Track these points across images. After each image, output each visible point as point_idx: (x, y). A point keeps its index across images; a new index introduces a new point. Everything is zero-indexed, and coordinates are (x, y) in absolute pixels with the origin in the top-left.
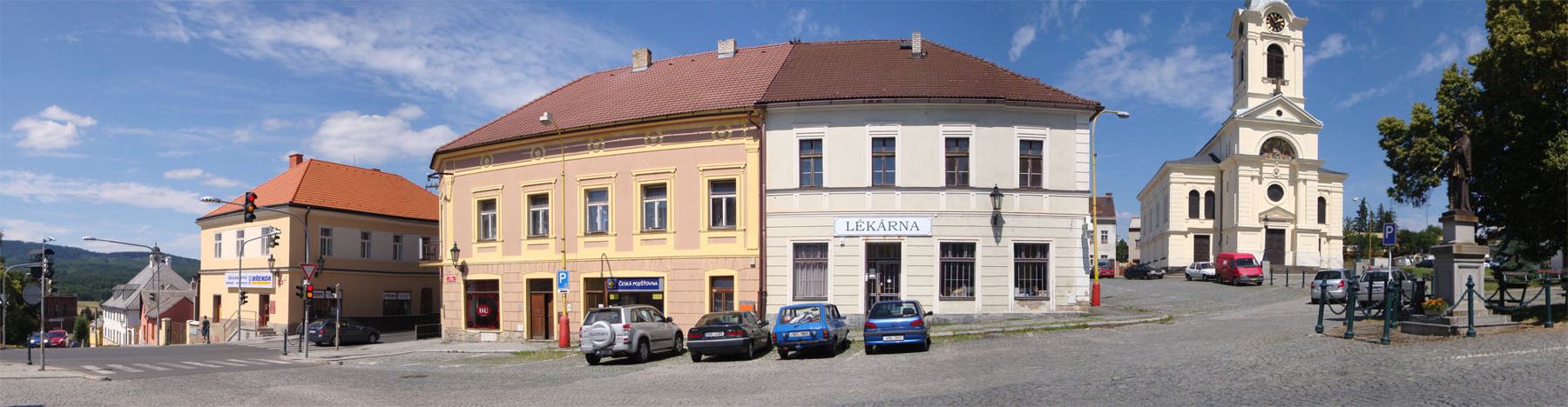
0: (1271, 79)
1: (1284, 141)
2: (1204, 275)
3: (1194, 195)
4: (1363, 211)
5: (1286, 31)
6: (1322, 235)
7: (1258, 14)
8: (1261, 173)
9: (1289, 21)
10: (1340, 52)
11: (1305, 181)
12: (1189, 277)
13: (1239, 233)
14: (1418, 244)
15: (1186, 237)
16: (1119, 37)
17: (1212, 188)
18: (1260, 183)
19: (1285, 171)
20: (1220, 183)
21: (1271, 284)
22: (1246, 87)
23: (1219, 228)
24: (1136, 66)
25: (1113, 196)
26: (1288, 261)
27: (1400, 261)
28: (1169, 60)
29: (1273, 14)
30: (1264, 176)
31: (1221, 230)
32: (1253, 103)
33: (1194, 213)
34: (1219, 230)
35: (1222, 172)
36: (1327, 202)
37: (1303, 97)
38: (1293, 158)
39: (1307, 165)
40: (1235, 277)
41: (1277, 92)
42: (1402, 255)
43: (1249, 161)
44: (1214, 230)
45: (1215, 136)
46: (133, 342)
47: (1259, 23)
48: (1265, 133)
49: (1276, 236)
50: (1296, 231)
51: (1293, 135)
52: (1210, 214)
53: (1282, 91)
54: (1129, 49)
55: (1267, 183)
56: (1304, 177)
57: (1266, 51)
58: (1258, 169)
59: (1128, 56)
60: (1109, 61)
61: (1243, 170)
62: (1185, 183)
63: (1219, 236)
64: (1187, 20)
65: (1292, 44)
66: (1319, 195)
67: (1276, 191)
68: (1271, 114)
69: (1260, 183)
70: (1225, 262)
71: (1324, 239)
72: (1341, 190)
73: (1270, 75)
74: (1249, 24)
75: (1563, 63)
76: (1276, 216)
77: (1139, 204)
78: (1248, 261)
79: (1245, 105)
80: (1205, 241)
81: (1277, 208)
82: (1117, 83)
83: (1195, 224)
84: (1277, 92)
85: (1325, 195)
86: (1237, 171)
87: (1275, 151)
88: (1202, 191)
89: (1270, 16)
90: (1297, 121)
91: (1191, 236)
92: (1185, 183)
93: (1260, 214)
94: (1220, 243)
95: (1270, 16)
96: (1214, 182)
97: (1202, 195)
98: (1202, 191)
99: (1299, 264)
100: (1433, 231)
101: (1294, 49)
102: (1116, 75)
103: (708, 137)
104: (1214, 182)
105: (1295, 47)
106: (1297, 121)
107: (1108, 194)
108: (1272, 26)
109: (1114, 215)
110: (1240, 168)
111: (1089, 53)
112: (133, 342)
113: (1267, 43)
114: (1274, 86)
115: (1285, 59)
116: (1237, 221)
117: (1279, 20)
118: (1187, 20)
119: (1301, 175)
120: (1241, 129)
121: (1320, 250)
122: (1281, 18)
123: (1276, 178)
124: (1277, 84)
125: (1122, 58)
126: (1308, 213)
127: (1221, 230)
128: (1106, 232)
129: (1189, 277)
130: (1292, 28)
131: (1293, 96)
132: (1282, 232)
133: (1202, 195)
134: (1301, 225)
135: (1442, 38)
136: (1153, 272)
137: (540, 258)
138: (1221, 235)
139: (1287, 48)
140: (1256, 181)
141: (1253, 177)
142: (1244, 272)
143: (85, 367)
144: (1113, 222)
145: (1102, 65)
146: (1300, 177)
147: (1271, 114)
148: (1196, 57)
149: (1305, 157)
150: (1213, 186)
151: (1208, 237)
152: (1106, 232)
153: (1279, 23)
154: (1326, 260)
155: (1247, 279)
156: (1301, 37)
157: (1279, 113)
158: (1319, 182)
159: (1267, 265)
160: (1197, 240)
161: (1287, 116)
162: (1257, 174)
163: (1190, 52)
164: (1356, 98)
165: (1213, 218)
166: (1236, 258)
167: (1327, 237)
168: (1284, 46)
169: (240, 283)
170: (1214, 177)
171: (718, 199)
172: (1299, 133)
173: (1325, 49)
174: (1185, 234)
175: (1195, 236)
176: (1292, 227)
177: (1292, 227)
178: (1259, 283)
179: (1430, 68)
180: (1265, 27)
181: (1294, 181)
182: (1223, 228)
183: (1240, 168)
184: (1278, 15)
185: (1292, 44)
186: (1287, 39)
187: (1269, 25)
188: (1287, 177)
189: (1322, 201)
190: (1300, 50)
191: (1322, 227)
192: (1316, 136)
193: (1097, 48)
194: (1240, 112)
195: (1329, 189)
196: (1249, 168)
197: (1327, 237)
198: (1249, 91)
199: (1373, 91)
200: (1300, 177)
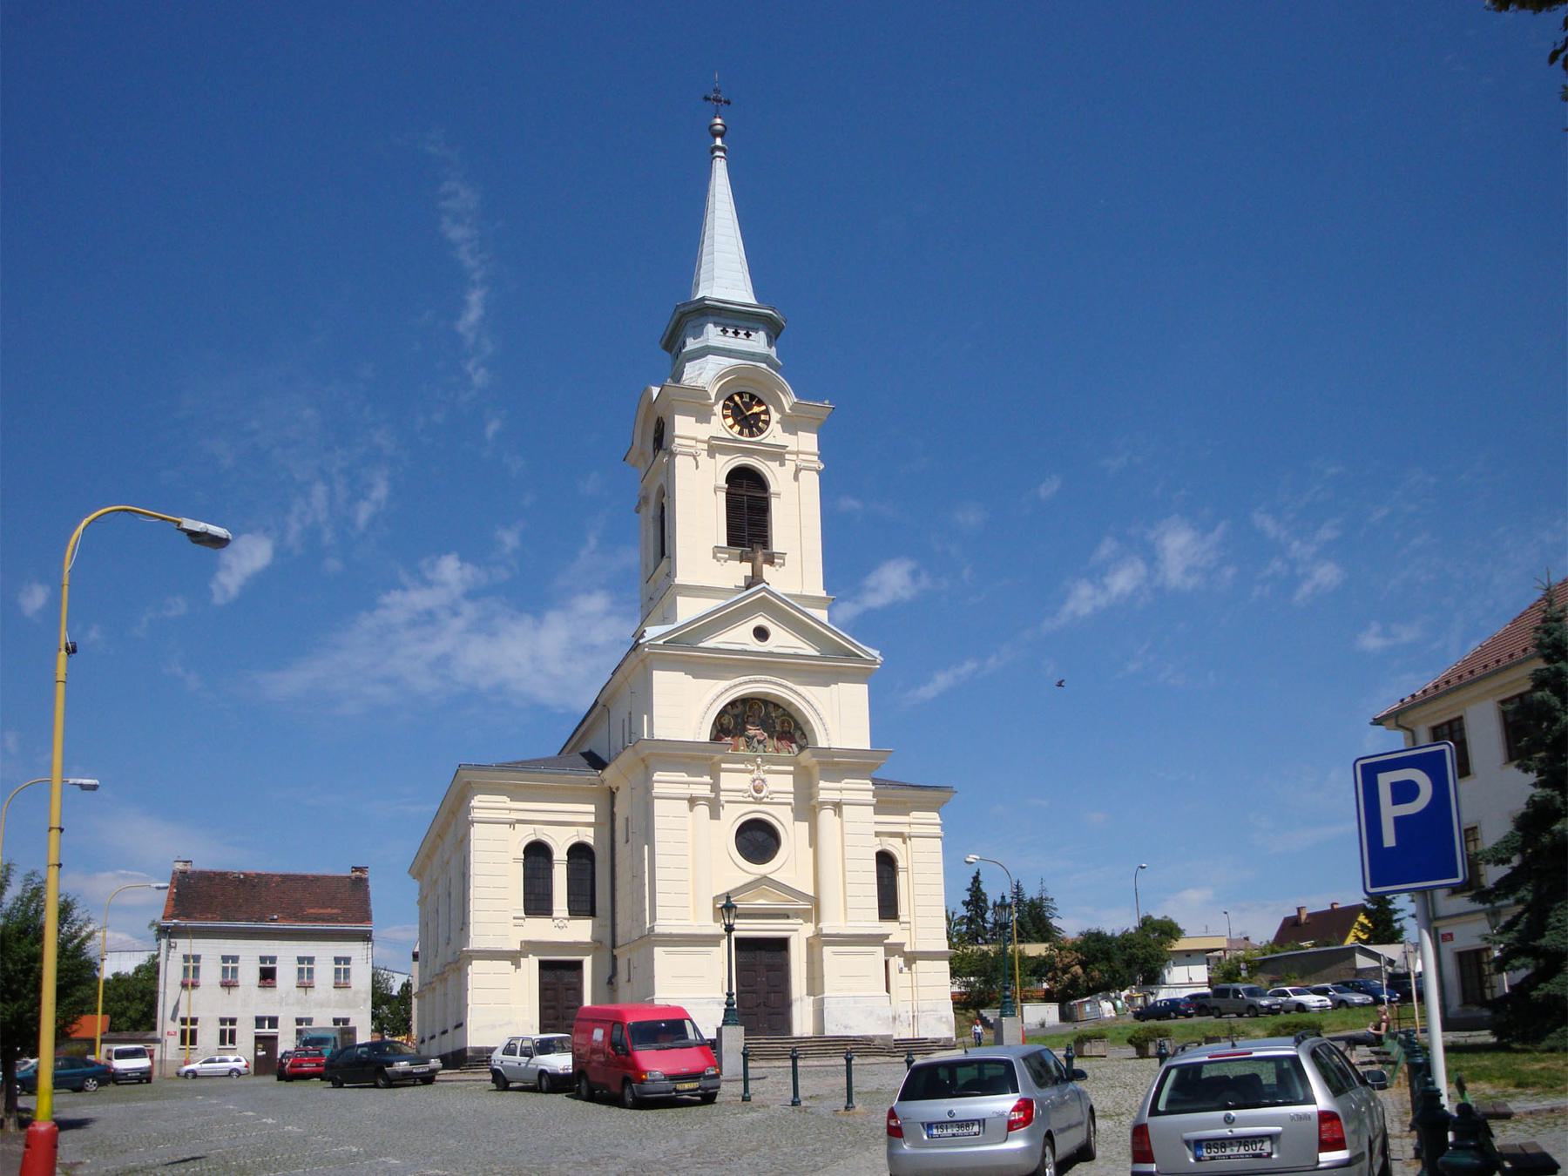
0: (737, 551)
1: (777, 706)
2: (542, 1073)
3: (537, 854)
4: (976, 899)
5: (774, 434)
6: (893, 950)
7: (702, 393)
8: (715, 788)
9: (780, 408)
10: (906, 595)
11: (837, 806)
12: (501, 1082)
13: (659, 952)
14: (1129, 963)
15: (518, 966)
16: (450, 569)
17: (588, 836)
18: (715, 814)
19: (781, 783)
20: (608, 821)
21: (746, 1099)
22: (671, 574)
23: (608, 942)
24: (484, 627)
25: (370, 875)
26: (802, 1023)
27: (1088, 1008)
28: (553, 617)
29: (740, 395)
30: (723, 797)
31: (614, 946)
32: (688, 610)
33: (537, 902)
34: (608, 946)
35: (612, 794)
36: (901, 863)
37: (823, 594)
38: (801, 748)
39: (842, 764)
40: (626, 1081)
41: (755, 580)
42: (1091, 992)
43: (681, 756)
44: (594, 947)
45: (596, 702)
47: (703, 416)
48: (723, 684)
49: (765, 957)
50: (819, 941)
51: (800, 689)
52: (582, 905)
53: (765, 577)
54: (472, 595)
55: (734, 817)
57: (723, 483)
58: (707, 779)
59: (469, 610)
60: (428, 618)
61: (666, 782)
62: (512, 824)
63: (608, 957)
64: (593, 542)
65: (790, 467)
66: (878, 845)
67: (760, 836)
68: (739, 637)
69: (715, 814)
70: (598, 1034)
71: (897, 962)
72: (937, 830)
73: (735, 538)
74: (678, 418)
75: (886, 941)
76: (761, 903)
77: (415, 885)
78: (672, 1028)
79: (669, 616)
80: (568, 976)
81: (765, 880)
82: (443, 661)
83: (541, 929)
84: (755, 580)
85: (893, 846)
86: (648, 785)
87: (752, 731)
88: (560, 845)
89: (731, 398)
90: (809, 650)
91: (531, 964)
92: (512, 824)
93: (715, 899)
94: (611, 981)
95: (731, 398)
96: (592, 819)
97: (560, 855)
98: (560, 845)
99: (832, 1030)
100: (1154, 930)
101: (796, 478)
102: (440, 646)
103: (822, 960)
104: (592, 819)
105: (798, 470)
106: (809, 650)
107: (357, 869)
108: (736, 422)
109: (366, 917)
110: (657, 776)
111: (387, 600)
113: (725, 464)
114: (746, 569)
115: (774, 503)
116: (653, 918)
117: (756, 409)
118: (593, 542)
119: (827, 791)
120: (658, 676)
121: (888, 990)
122: (760, 403)
123: (758, 801)
124: (752, 560)
125: (456, 613)
126: (851, 890)
127: (614, 946)
128: (347, 960)
129: (501, 1082)
130: (790, 426)
131: (796, 591)
132: (782, 945)
133: (560, 855)
134: (830, 925)
135: (1107, 548)
136: (402, 1066)
137: (265, 1002)
138: (614, 958)
139: (777, 477)
140: (703, 810)
141: (693, 801)
142: (656, 1064)
144: (366, 937)
145: (412, 624)
146: (823, 796)
147: (739, 637)
148: (609, 613)
149: (836, 744)
150: (591, 831)
151: (578, 966)
152: (347, 960)
153: (758, 414)
154: (906, 1016)
155: (668, 1085)
156: (815, 449)
158: (879, 810)
159: (735, 1039)
160: (550, 975)
161: (782, 640)
162: (705, 791)
163: (596, 603)
164: (942, 680)
165: (592, 913)
166: (630, 1021)
167: (904, 954)
168: (769, 469)
170: (592, 808)
172: (772, 461)
173: (875, 590)
174: (514, 957)
175: (541, 962)
176: (808, 929)
177: (808, 929)
178: (708, 1098)
179: (1086, 609)
180: (720, 425)
181: (807, 808)
182: (619, 941)
183: (657, 776)
184: (752, 397)
185: (790, 467)
186: (777, 454)
187: (730, 421)
188: (790, 798)
189: (886, 862)
190: (811, 482)
191: (888, 927)
192: (862, 689)
193: (404, 589)
194: (652, 632)
195: (905, 829)
196: (683, 777)
197: (904, 954)
198: (679, 580)
199: (970, 666)
200: (823, 796)
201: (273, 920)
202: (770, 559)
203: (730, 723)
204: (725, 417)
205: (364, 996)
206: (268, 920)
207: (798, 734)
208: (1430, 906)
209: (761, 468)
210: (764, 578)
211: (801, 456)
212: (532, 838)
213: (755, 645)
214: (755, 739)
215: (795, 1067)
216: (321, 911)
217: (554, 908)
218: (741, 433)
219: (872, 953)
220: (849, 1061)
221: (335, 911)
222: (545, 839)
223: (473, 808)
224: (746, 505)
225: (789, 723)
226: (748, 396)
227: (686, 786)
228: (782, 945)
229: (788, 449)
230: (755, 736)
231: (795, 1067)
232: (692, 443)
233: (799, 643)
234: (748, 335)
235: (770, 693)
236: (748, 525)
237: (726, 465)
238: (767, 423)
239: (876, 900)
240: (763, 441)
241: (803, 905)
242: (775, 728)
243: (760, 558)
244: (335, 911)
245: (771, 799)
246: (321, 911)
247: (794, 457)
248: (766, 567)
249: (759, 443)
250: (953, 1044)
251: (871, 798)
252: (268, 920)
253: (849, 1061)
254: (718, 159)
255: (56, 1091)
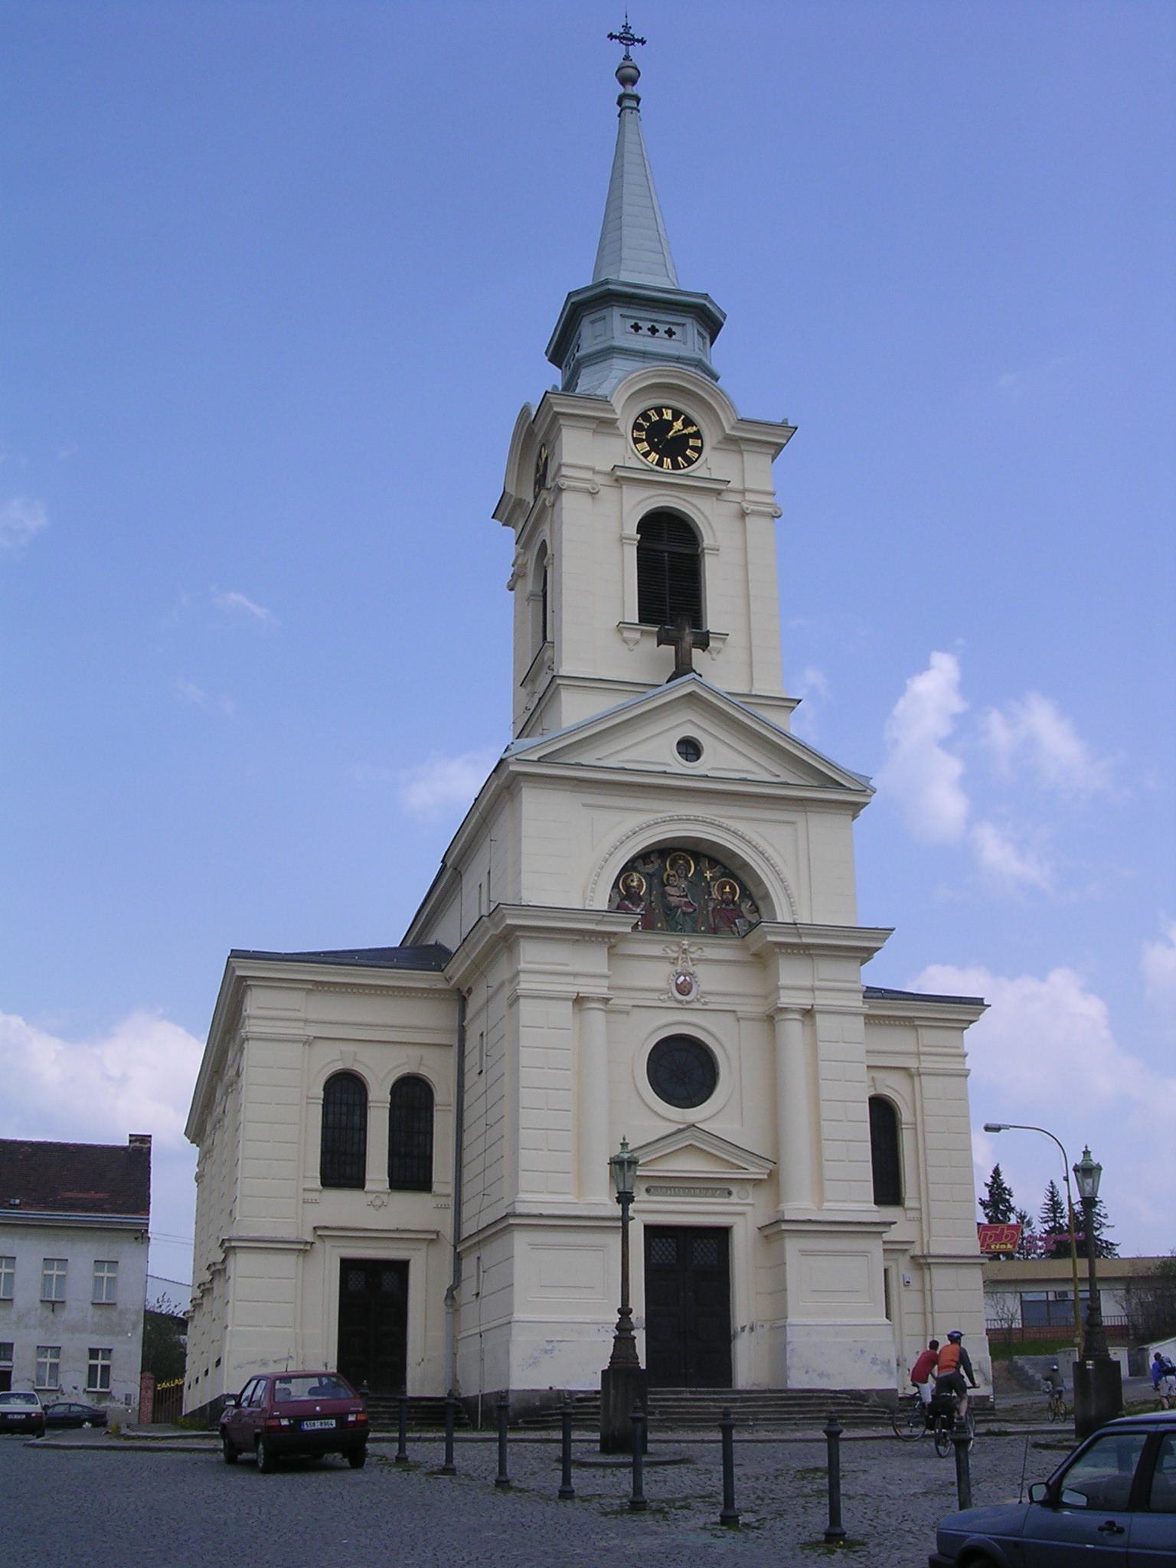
11: (808, 1013)
41: (683, 667)
46: (599, 1417)
50: (774, 1231)
56: (804, 1000)
57: (632, 530)
71: (902, 1268)
73: (647, 614)
85: (894, 1088)
92: (309, 1042)
108: (654, 448)
112: (599, 1417)
113: (639, 503)
123: (683, 1008)
134: (799, 1205)
143: (1111, 1422)
157: (690, 748)
168: (706, 515)
169: (566, 1442)
171: (94, 1359)
174: (303, 1249)
191: (889, 1213)
201: (15, 1206)
202: (703, 641)
203: (640, 885)
204: (636, 441)
205: (133, 1317)
206: (6, 1204)
207: (745, 907)
208: (824, 1253)
209: (692, 515)
210: (694, 667)
211: (749, 497)
212: (339, 1066)
213: (679, 765)
214: (680, 910)
215: (727, 1443)
216: (81, 1195)
217: (367, 1177)
218: (660, 463)
219: (864, 1254)
220: (833, 1437)
221: (101, 1195)
222: (358, 1068)
223: (249, 1017)
224: (667, 566)
225: (732, 888)
226: (670, 412)
227: (570, 979)
228: (721, 1235)
229: (730, 485)
230: (678, 907)
231: (727, 1443)
232: (588, 475)
233: (742, 763)
234: (670, 333)
235: (702, 840)
236: (670, 595)
237: (647, 502)
238: (699, 450)
239: (869, 1167)
240: (692, 474)
241: (755, 1172)
242: (710, 894)
243: (688, 639)
244: (101, 1195)
245: (706, 1003)
246: (81, 1195)
247: (737, 498)
248: (696, 653)
249: (687, 476)
250: (988, 1405)
251: (860, 1004)
252: (6, 1204)
253: (833, 1437)
254: (628, 111)
255: (9, 1369)
